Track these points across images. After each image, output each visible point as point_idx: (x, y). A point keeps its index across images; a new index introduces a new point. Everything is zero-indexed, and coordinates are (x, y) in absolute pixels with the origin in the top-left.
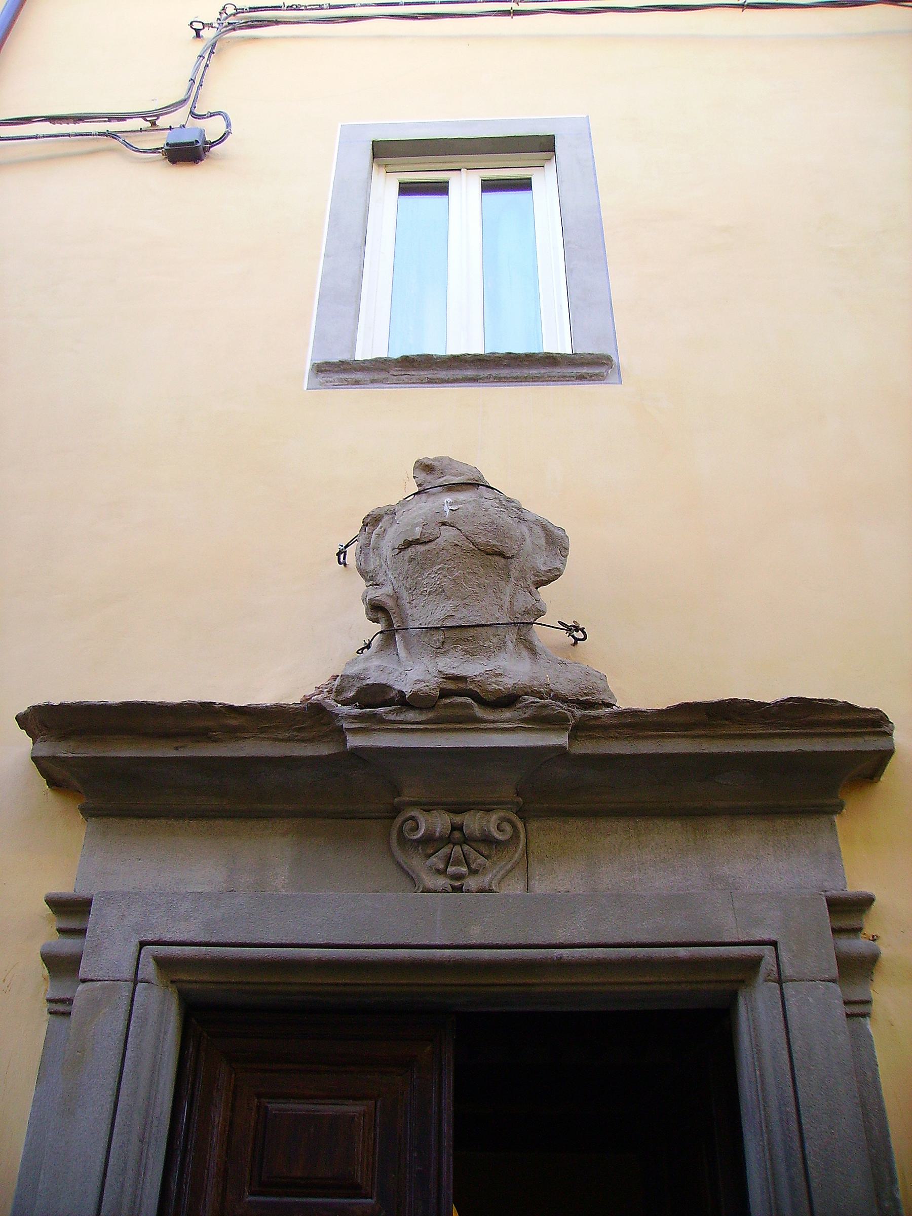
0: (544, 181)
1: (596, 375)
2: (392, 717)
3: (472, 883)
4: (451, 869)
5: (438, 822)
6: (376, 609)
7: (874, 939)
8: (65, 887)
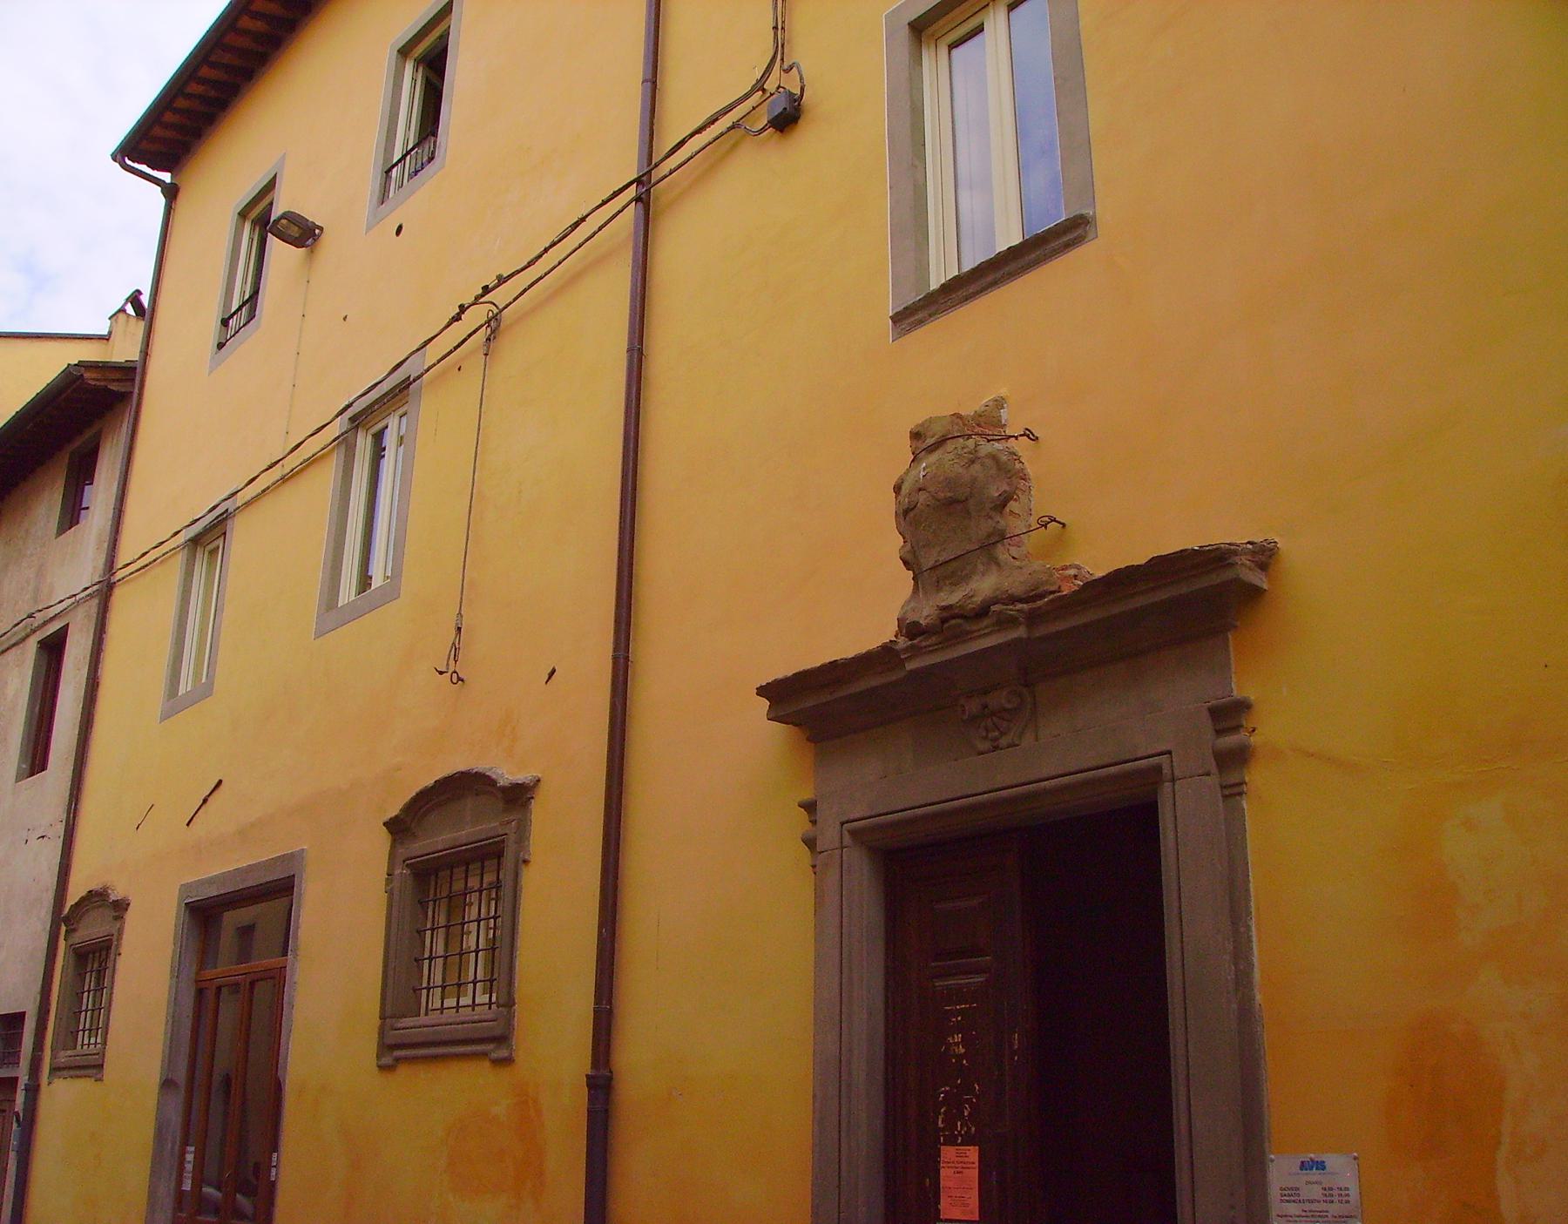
3: (1003, 741)
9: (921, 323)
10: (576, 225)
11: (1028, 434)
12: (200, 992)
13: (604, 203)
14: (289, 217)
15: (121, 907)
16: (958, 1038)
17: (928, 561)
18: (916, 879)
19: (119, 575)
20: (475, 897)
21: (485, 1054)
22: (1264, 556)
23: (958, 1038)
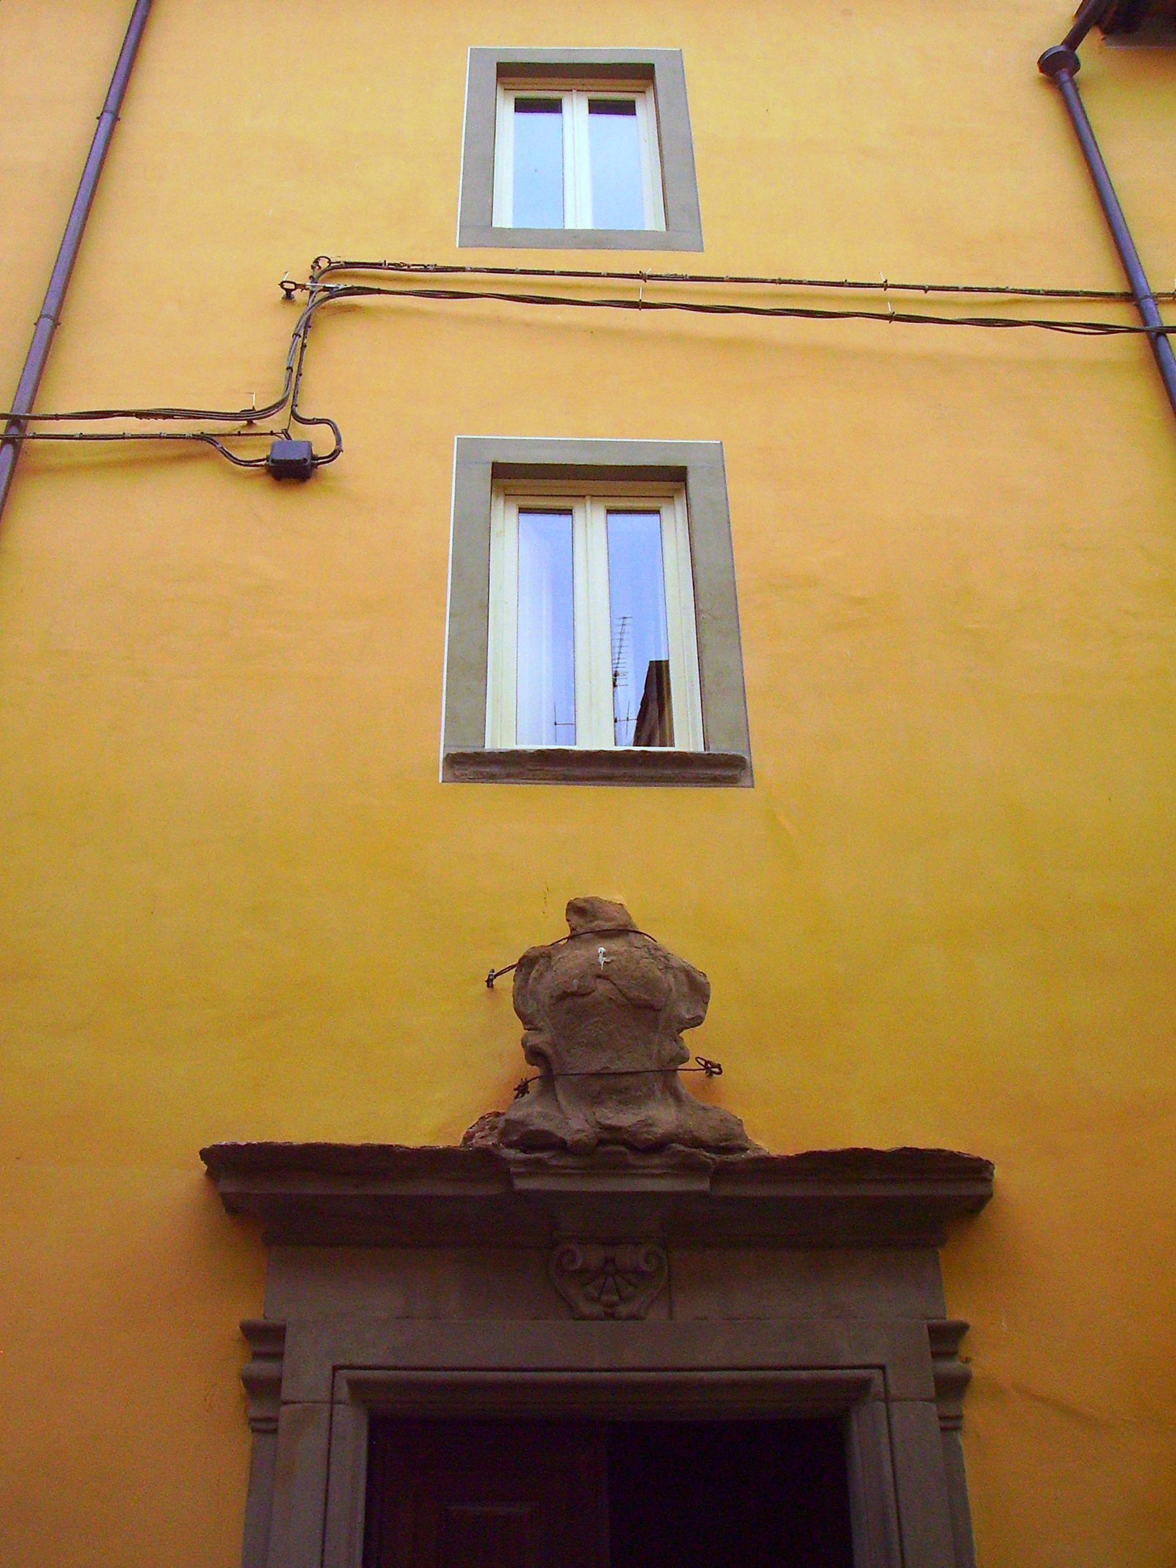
0: (645, 108)
2: (554, 1162)
3: (623, 1310)
4: (604, 1298)
5: (594, 1257)
6: (534, 1055)
7: (967, 1360)
8: (253, 1314)
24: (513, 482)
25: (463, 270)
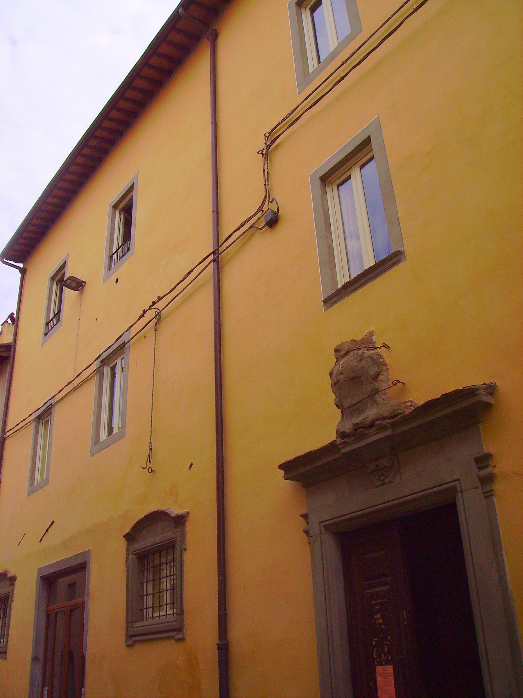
1: (396, 261)
2: (348, 441)
3: (386, 481)
9: (335, 302)
10: (189, 273)
11: (385, 346)
12: (48, 616)
13: (200, 263)
14: (71, 278)
15: (13, 579)
16: (379, 616)
17: (347, 404)
18: (354, 544)
19: (8, 434)
20: (165, 566)
21: (172, 637)
22: (491, 389)
23: (379, 616)
24: (331, 178)
25: (299, 106)
